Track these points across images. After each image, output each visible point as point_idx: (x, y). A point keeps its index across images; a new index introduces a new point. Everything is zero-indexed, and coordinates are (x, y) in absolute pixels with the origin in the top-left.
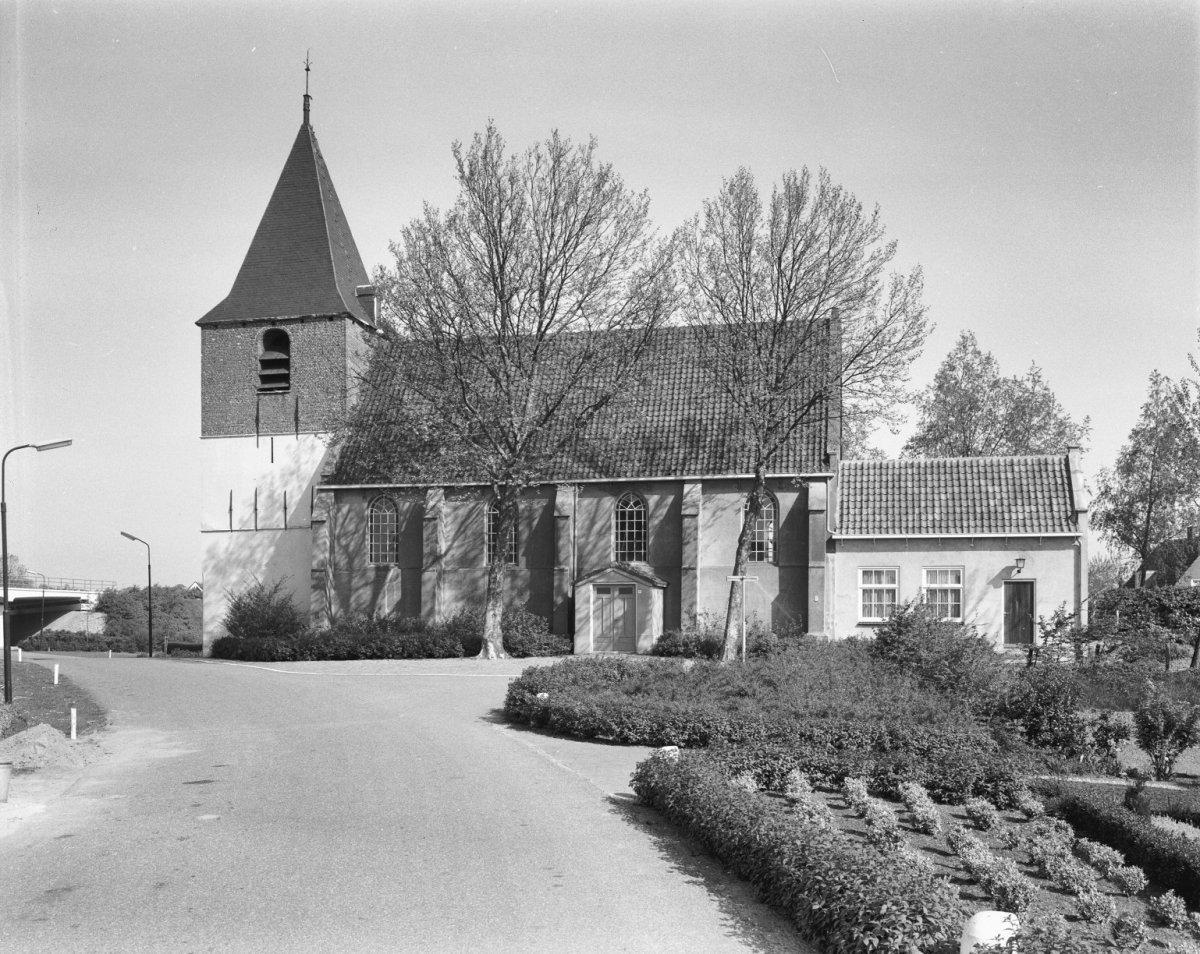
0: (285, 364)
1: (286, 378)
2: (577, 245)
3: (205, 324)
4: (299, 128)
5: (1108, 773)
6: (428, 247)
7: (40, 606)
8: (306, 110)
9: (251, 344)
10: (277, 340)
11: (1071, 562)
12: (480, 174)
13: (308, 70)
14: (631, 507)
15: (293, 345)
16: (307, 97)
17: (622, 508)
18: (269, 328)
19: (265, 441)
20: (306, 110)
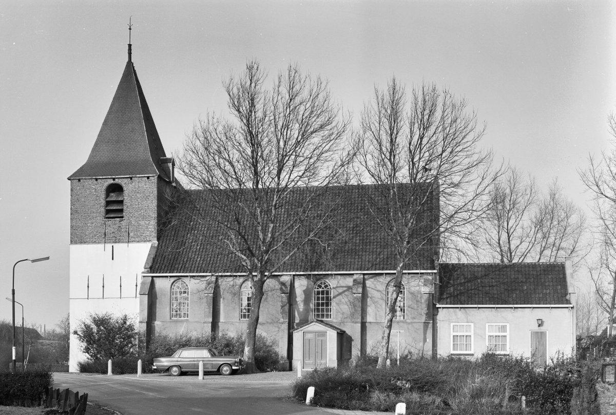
0: (121, 202)
1: (121, 211)
2: (421, 150)
3: (76, 177)
4: (125, 64)
5: (225, 355)
6: (210, 146)
7: (196, 373)
8: (130, 54)
9: (97, 189)
10: (116, 189)
11: (158, 279)
12: (245, 102)
13: (130, 29)
14: (323, 288)
15: (126, 192)
16: (130, 46)
17: (317, 289)
18: (112, 181)
19: (109, 246)
20: (130, 54)
